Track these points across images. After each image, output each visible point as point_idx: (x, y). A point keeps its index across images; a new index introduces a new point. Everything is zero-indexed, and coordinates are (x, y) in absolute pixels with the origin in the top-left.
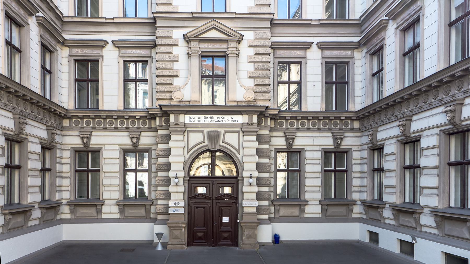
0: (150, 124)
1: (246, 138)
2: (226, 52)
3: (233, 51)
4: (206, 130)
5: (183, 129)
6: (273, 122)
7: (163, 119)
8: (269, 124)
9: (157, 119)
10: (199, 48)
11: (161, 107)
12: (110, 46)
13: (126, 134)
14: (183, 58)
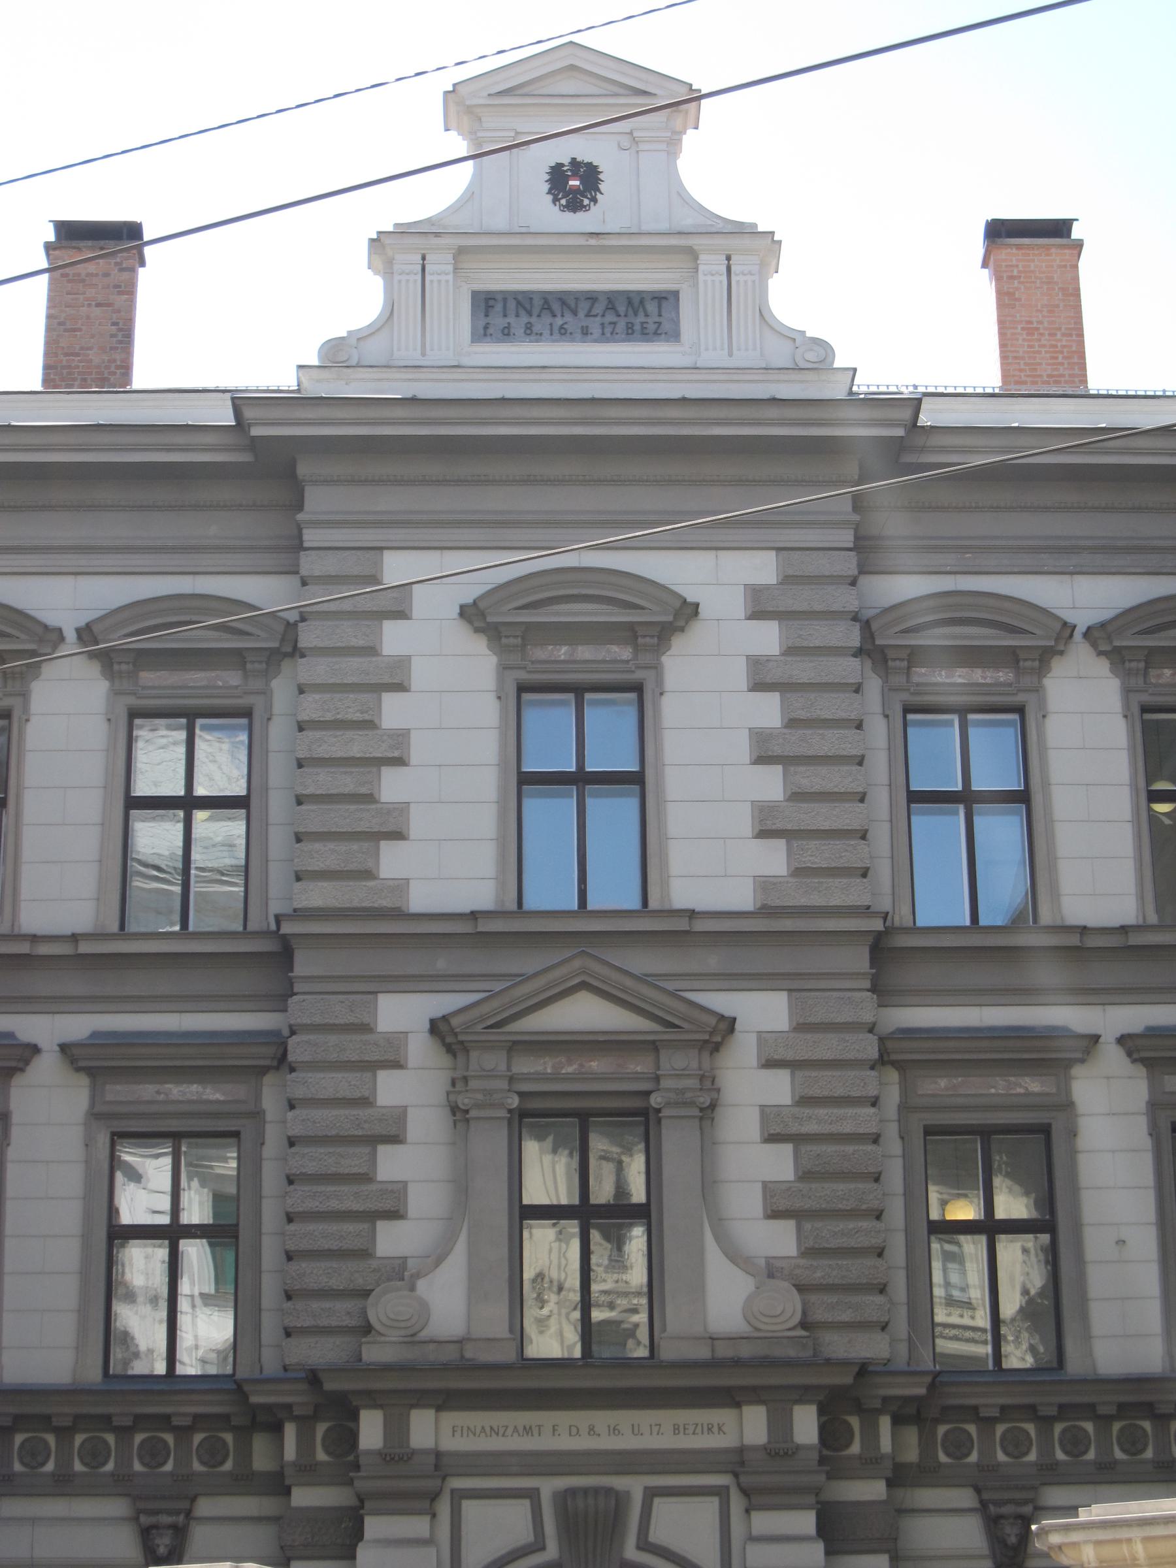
0: (245, 1453)
1: (765, 1522)
2: (647, 1094)
3: (682, 1091)
4: (549, 1487)
5: (423, 1484)
6: (911, 1435)
7: (321, 1429)
8: (886, 1444)
9: (290, 1431)
10: (511, 1079)
11: (313, 1378)
12: (47, 1066)
13: (117, 1507)
14: (427, 1123)
